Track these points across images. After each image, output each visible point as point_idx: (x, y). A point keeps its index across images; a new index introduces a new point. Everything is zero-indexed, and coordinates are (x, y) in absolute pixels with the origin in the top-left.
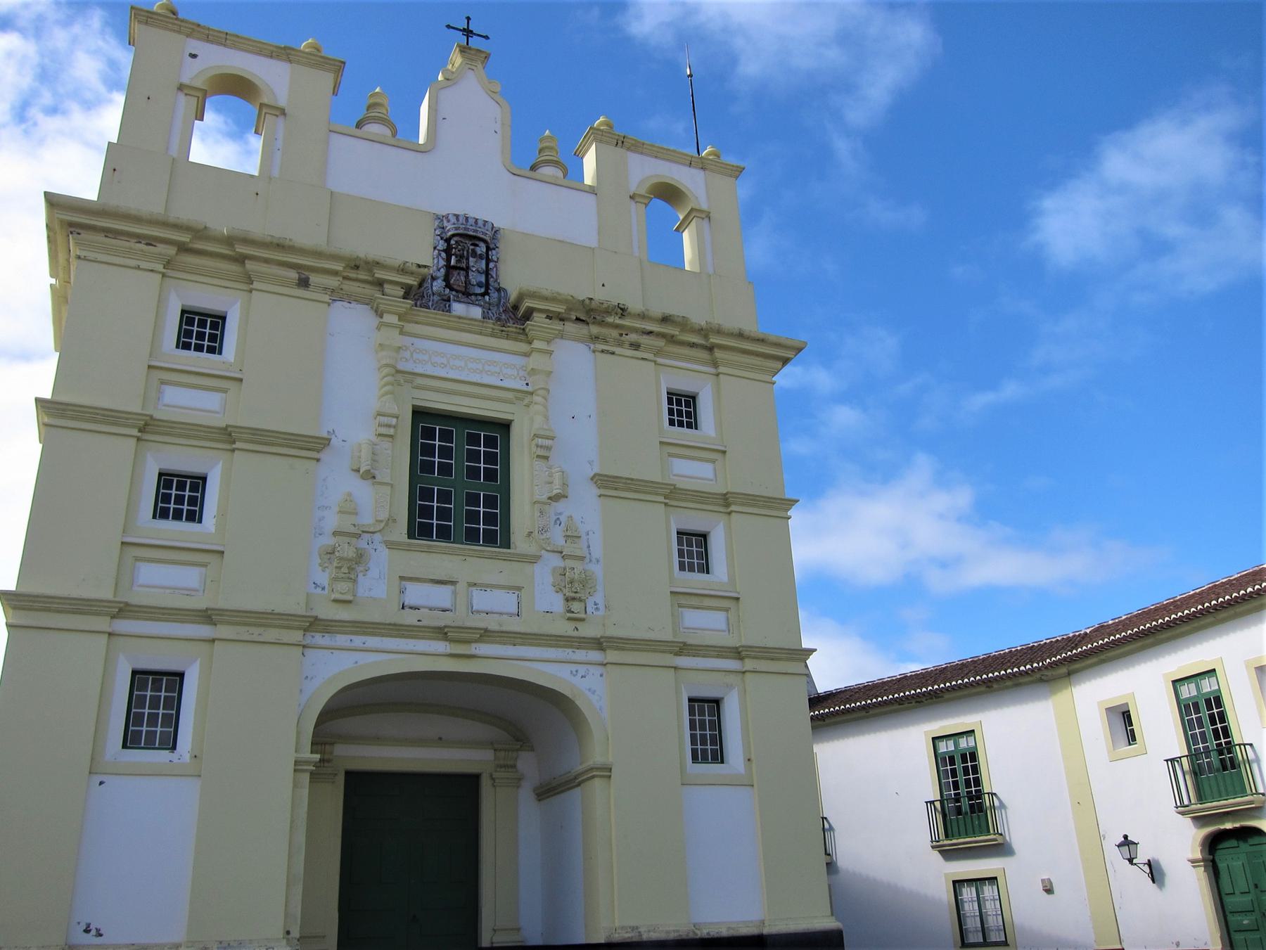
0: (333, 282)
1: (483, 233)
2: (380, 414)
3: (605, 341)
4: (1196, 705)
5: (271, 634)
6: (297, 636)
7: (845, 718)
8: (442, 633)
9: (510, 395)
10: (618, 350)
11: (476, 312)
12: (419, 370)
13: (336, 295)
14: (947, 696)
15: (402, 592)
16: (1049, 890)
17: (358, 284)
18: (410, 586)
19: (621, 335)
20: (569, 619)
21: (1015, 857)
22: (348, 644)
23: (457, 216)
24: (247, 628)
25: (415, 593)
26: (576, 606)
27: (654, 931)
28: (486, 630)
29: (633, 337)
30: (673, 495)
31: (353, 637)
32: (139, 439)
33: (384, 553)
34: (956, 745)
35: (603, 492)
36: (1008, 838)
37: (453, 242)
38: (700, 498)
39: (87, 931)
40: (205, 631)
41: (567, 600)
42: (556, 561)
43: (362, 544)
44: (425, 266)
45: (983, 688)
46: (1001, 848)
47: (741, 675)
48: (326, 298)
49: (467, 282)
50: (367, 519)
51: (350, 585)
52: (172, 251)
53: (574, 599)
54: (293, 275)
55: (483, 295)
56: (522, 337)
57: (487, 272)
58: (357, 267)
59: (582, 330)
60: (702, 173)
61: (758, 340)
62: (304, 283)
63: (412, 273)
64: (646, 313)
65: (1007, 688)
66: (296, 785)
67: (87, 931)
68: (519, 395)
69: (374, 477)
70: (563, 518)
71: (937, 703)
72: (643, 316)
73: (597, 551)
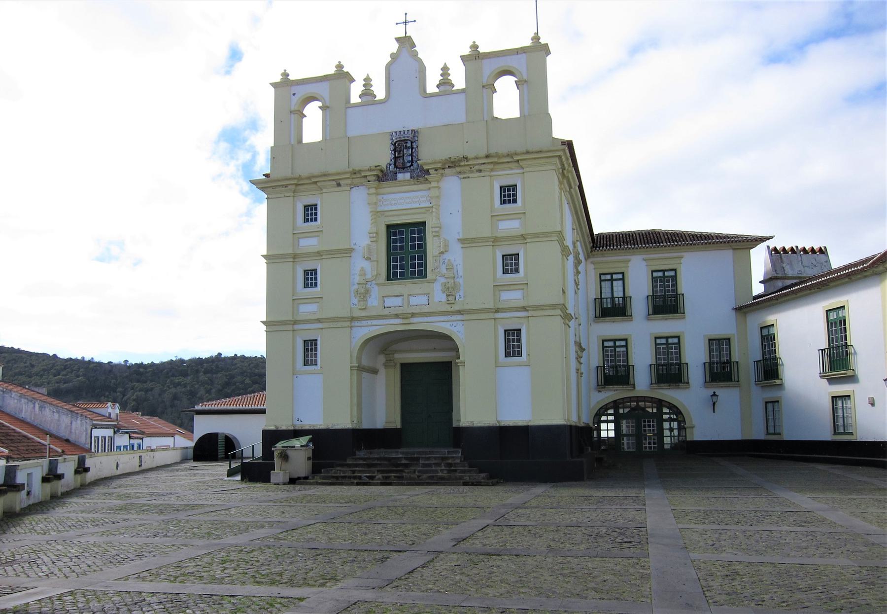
0: (349, 181)
1: (408, 137)
2: (369, 233)
3: (465, 173)
4: (835, 323)
5: (339, 324)
6: (348, 324)
7: (785, 299)
8: (397, 316)
9: (423, 210)
10: (470, 175)
11: (408, 175)
12: (386, 209)
13: (352, 186)
14: (832, 284)
15: (384, 302)
16: (873, 404)
17: (358, 179)
18: (386, 299)
19: (471, 168)
20: (448, 304)
21: (859, 384)
22: (366, 324)
23: (396, 132)
24: (331, 323)
25: (389, 302)
26: (450, 298)
27: (480, 423)
28: (413, 313)
29: (477, 167)
30: (496, 241)
31: (368, 321)
32: (293, 262)
33: (376, 287)
34: (838, 315)
35: (463, 246)
36: (856, 373)
37: (396, 145)
38: (510, 239)
39: (298, 420)
40: (320, 325)
41: (447, 296)
42: (443, 280)
43: (368, 286)
44: (378, 166)
45: (847, 280)
46: (852, 379)
47: (527, 318)
48: (348, 188)
49: (404, 163)
50: (369, 276)
51: (365, 302)
52: (293, 187)
53: (449, 295)
54: (334, 183)
55: (410, 166)
56: (427, 182)
57: (412, 155)
58: (355, 173)
59: (453, 171)
60: (524, 55)
61: (538, 152)
62: (339, 185)
63: (375, 170)
64: (477, 156)
65: (860, 279)
66: (352, 374)
67: (298, 420)
68: (427, 209)
69: (370, 259)
70: (446, 261)
71: (827, 289)
72: (476, 158)
73: (461, 273)
